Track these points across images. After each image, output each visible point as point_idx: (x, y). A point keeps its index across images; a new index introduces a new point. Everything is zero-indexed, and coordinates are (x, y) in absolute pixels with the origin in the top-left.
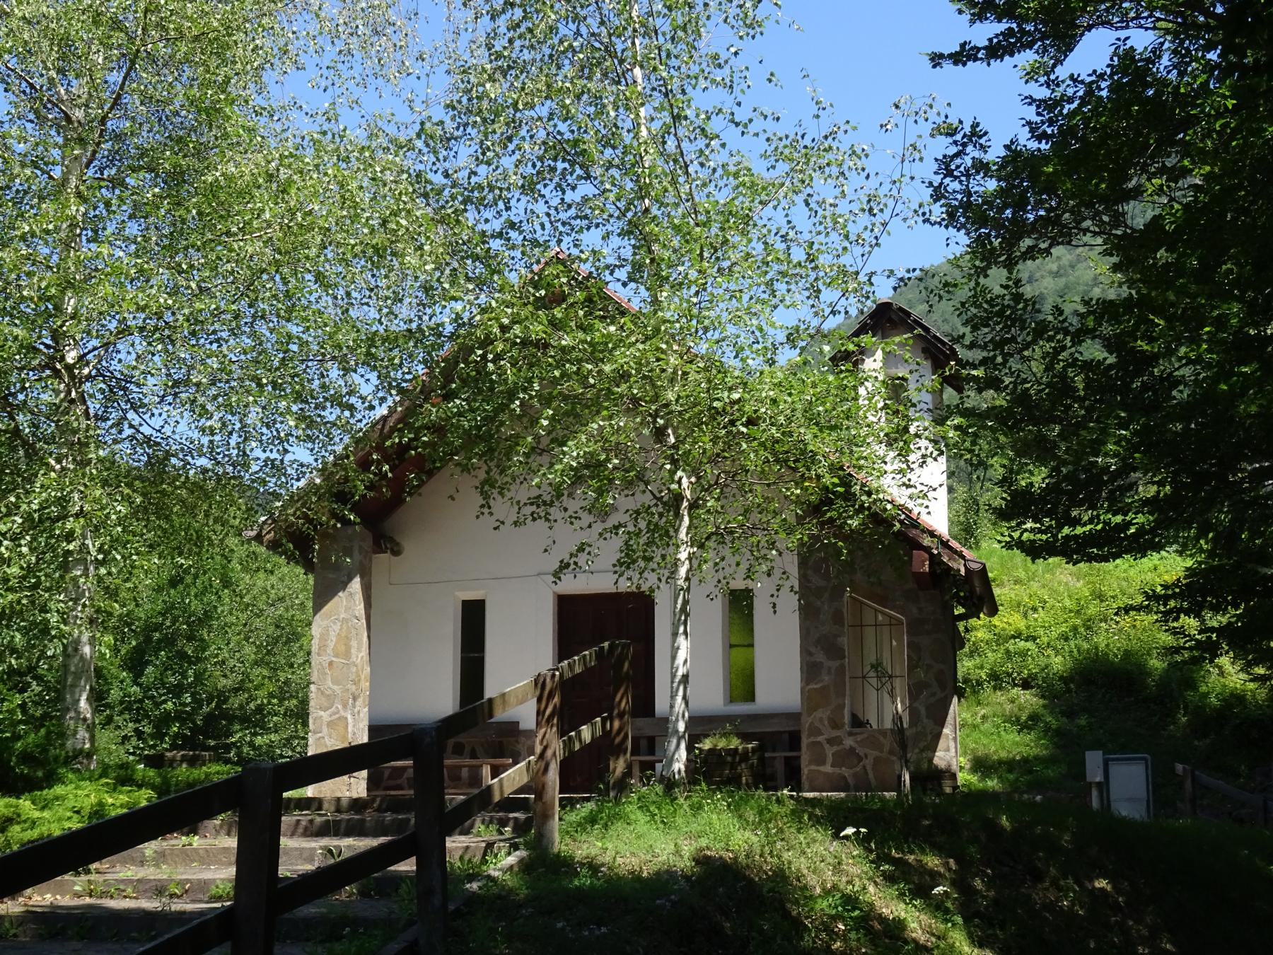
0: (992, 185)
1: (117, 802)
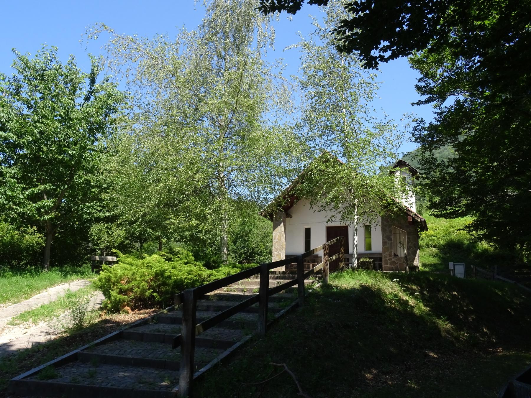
0: (426, 132)
1: (234, 272)
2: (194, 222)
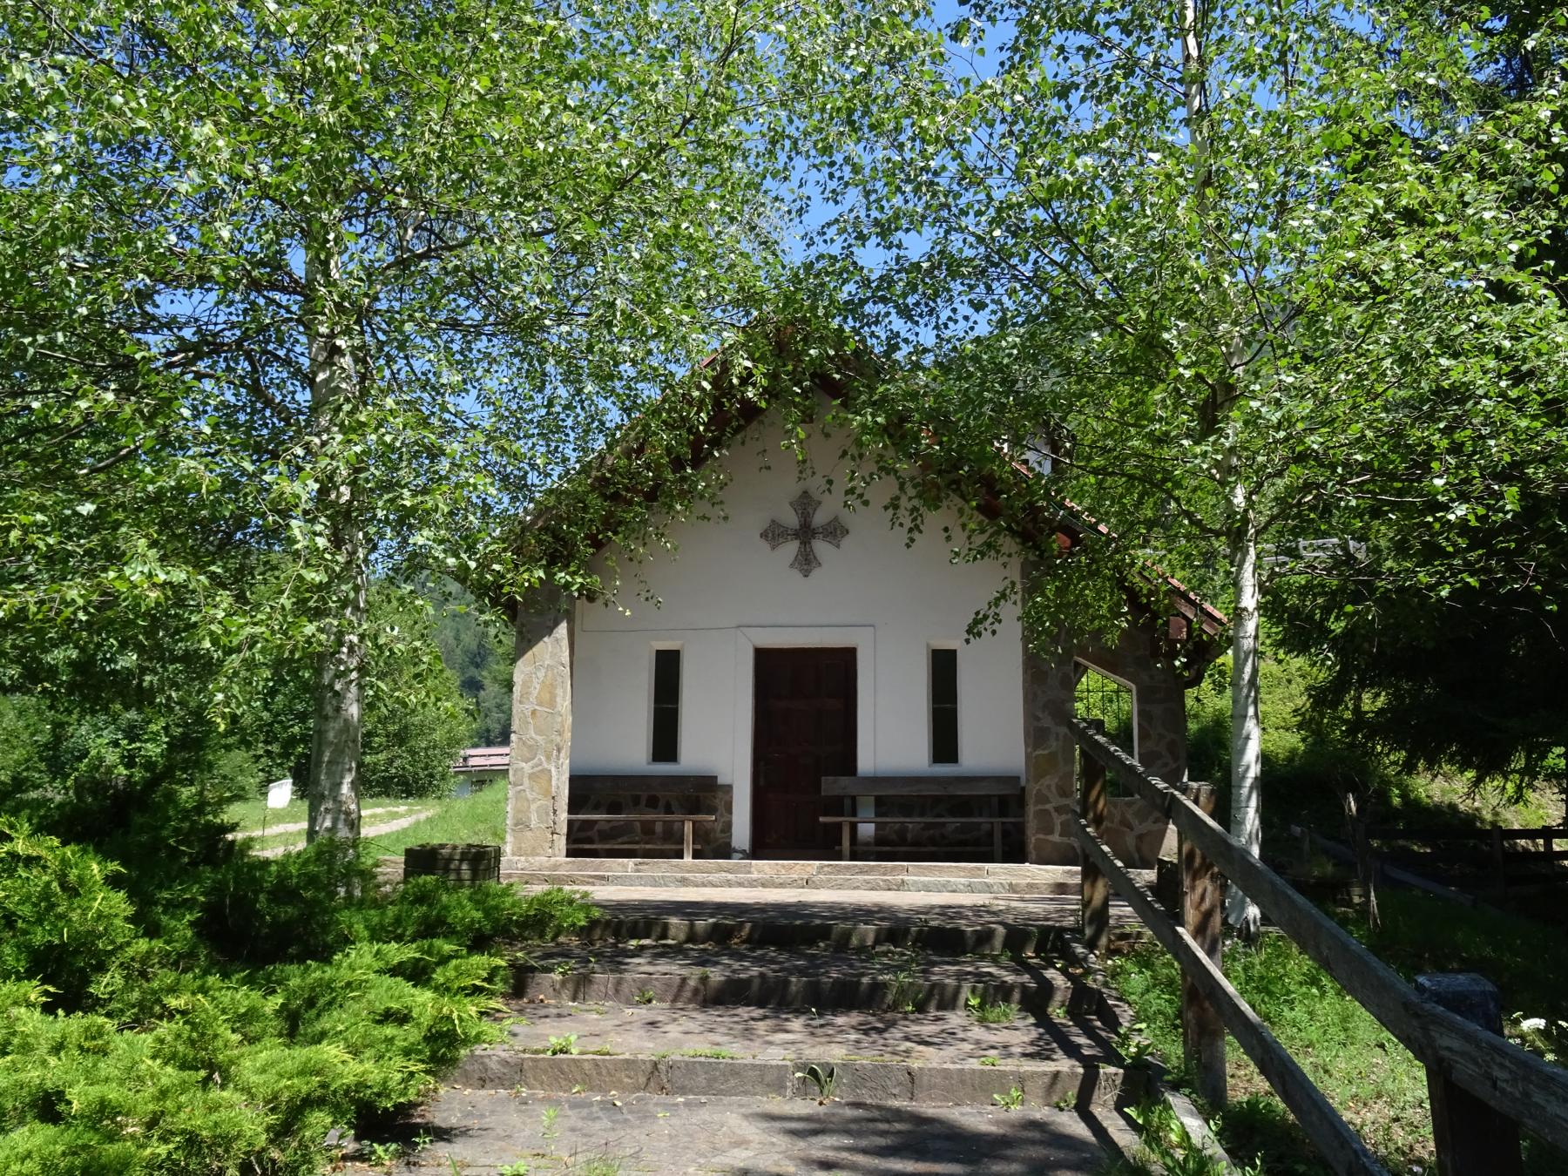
2: (145, 572)
